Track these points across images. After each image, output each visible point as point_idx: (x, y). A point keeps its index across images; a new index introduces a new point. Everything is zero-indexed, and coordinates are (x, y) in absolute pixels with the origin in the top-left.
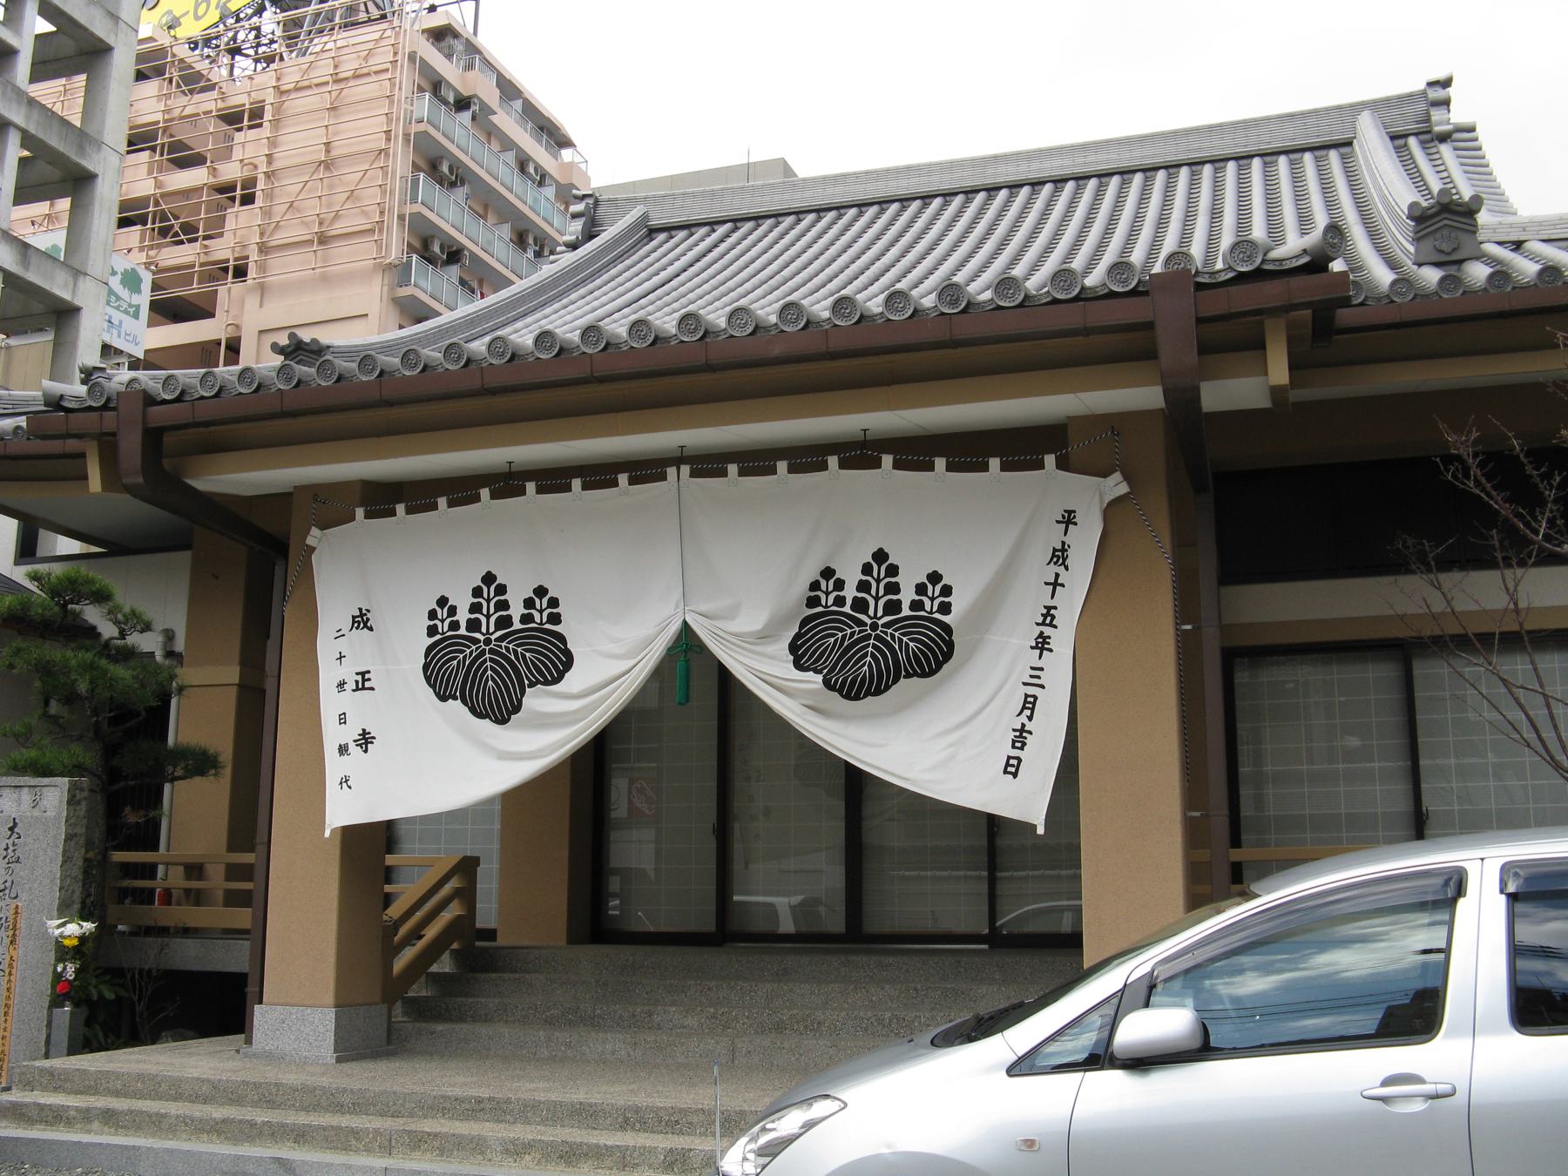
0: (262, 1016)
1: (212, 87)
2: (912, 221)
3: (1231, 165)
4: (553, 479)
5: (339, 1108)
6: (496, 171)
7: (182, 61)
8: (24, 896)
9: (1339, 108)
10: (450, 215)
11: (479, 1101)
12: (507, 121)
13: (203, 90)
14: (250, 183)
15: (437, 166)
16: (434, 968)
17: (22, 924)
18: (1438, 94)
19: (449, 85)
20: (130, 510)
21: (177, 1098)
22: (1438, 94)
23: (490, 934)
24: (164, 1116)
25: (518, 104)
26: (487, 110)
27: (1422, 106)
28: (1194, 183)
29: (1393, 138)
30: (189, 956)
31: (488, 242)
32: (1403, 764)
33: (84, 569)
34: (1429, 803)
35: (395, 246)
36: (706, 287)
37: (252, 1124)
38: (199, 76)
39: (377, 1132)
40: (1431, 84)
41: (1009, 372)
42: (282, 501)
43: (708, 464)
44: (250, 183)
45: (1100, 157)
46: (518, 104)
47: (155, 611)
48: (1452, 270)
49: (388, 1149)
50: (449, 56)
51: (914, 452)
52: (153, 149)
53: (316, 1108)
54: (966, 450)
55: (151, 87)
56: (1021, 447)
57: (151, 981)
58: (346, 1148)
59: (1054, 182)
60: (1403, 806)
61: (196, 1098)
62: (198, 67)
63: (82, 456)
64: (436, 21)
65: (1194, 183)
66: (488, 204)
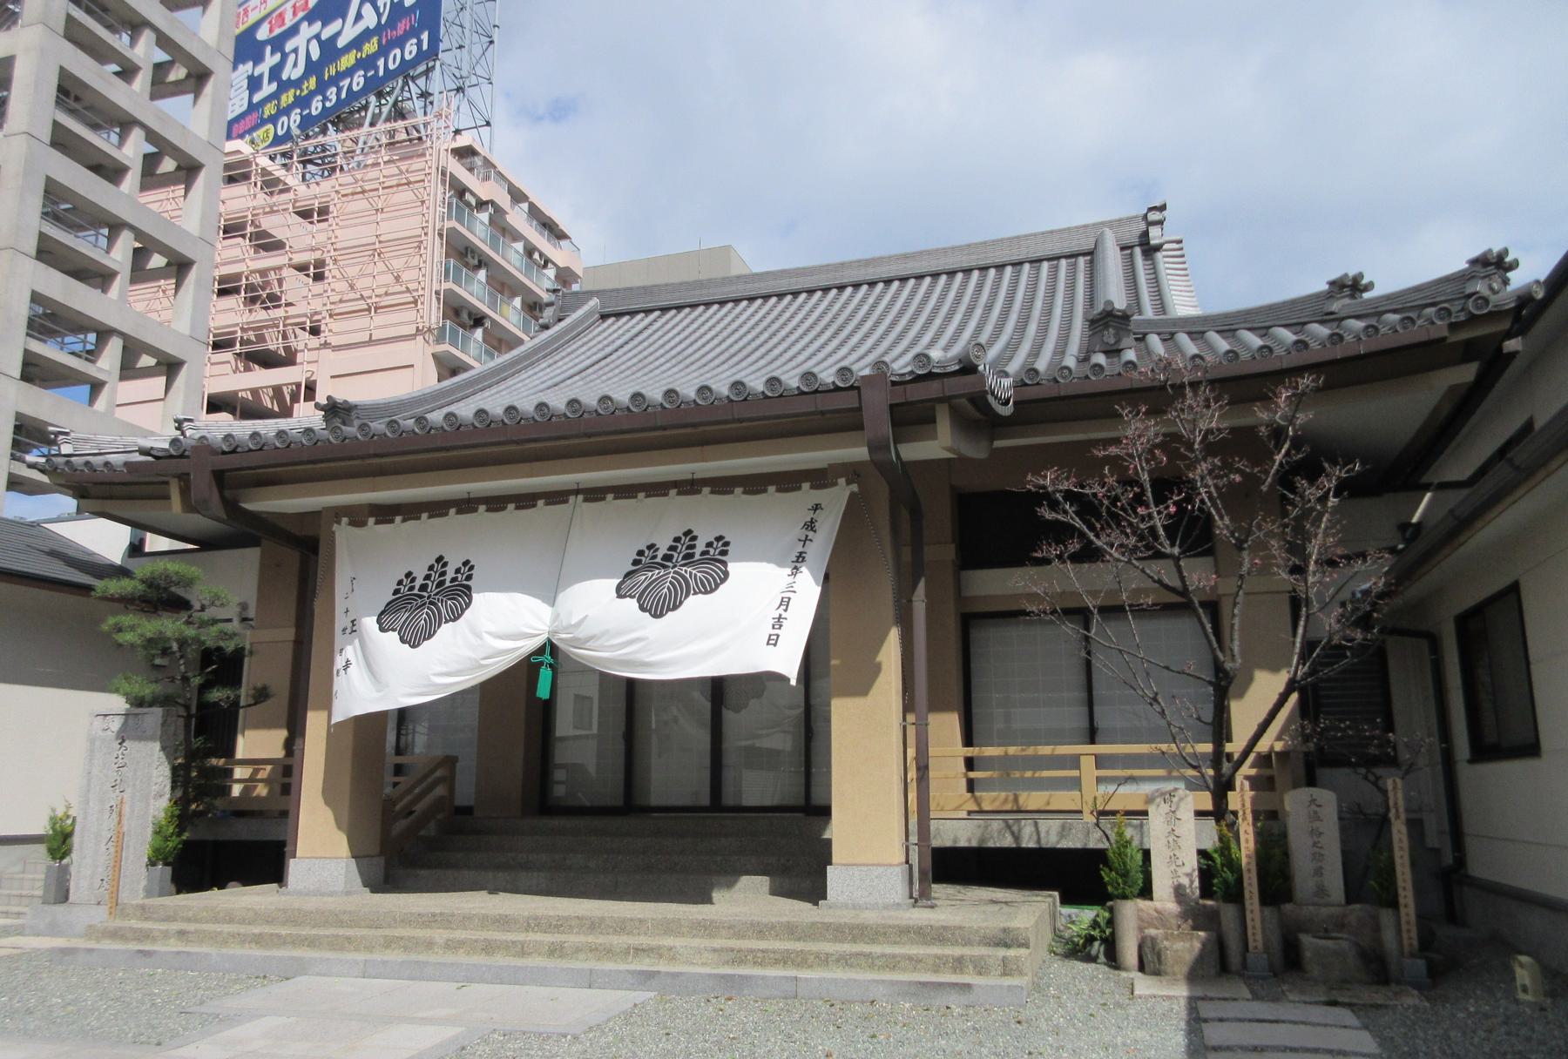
0: (294, 868)
1: (287, 190)
2: (831, 305)
3: (1045, 265)
4: (496, 503)
5: (341, 924)
6: (511, 259)
7: (263, 169)
8: (129, 790)
9: (1085, 226)
10: (475, 291)
11: (434, 915)
12: (517, 218)
13: (282, 191)
14: (320, 264)
15: (463, 255)
16: (422, 833)
17: (126, 809)
18: (1153, 216)
19: (472, 193)
20: (199, 522)
21: (231, 921)
22: (1153, 216)
23: (468, 811)
24: (220, 933)
25: (525, 206)
26: (499, 211)
27: (1143, 226)
28: (1073, 270)
29: (1123, 249)
30: (244, 831)
31: (510, 316)
32: (1084, 695)
33: (172, 566)
34: (1100, 722)
35: (432, 314)
36: (674, 352)
37: (279, 936)
38: (277, 181)
39: (363, 937)
40: (1151, 209)
41: (425, 470)
42: (314, 516)
43: (594, 494)
44: (320, 264)
45: (749, 286)
46: (525, 206)
47: (229, 589)
48: (1373, 321)
49: (370, 949)
50: (471, 170)
51: (722, 485)
52: (243, 236)
53: (326, 923)
54: (755, 484)
55: (240, 189)
56: (787, 481)
57: (220, 846)
58: (342, 949)
59: (1013, 265)
60: (1085, 724)
61: (242, 922)
62: (277, 174)
63: (167, 483)
64: (463, 141)
65: (1073, 270)
66: (503, 285)
